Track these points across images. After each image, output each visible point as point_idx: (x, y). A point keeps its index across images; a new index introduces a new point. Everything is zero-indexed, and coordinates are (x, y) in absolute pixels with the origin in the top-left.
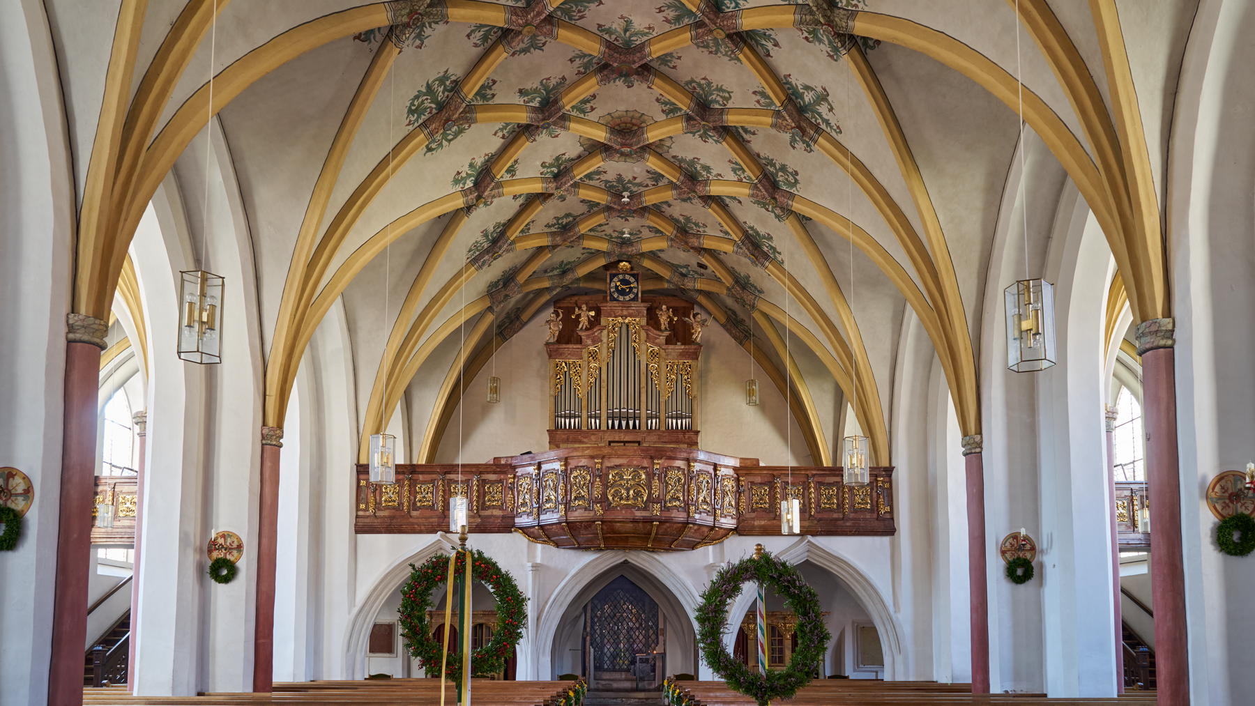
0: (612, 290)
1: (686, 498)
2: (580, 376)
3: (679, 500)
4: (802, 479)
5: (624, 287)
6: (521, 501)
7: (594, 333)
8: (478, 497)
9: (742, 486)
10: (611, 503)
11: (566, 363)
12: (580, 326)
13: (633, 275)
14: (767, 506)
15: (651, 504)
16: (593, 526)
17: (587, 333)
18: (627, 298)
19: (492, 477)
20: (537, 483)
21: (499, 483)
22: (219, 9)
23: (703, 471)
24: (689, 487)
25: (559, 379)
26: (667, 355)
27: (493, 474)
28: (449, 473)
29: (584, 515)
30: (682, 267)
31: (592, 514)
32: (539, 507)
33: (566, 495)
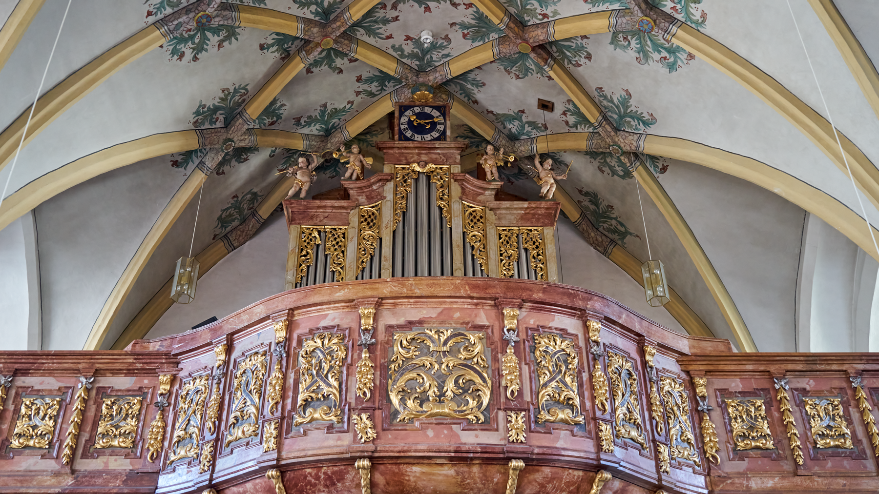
0: (402, 127)
1: (588, 404)
2: (343, 252)
3: (572, 407)
4: (837, 383)
5: (422, 122)
6: (178, 432)
7: (371, 185)
8: (80, 427)
9: (703, 398)
10: (397, 412)
11: (319, 232)
12: (347, 174)
13: (438, 108)
14: (770, 444)
15: (501, 414)
16: (349, 477)
17: (358, 184)
18: (428, 137)
19: (122, 382)
20: (219, 384)
21: (134, 396)
22: (39, 101)
23: (617, 348)
24: (591, 377)
25: (305, 256)
26: (499, 219)
27: (126, 375)
28: (25, 372)
29: (326, 444)
30: (511, 118)
31: (346, 440)
32: (217, 440)
33: (283, 397)
